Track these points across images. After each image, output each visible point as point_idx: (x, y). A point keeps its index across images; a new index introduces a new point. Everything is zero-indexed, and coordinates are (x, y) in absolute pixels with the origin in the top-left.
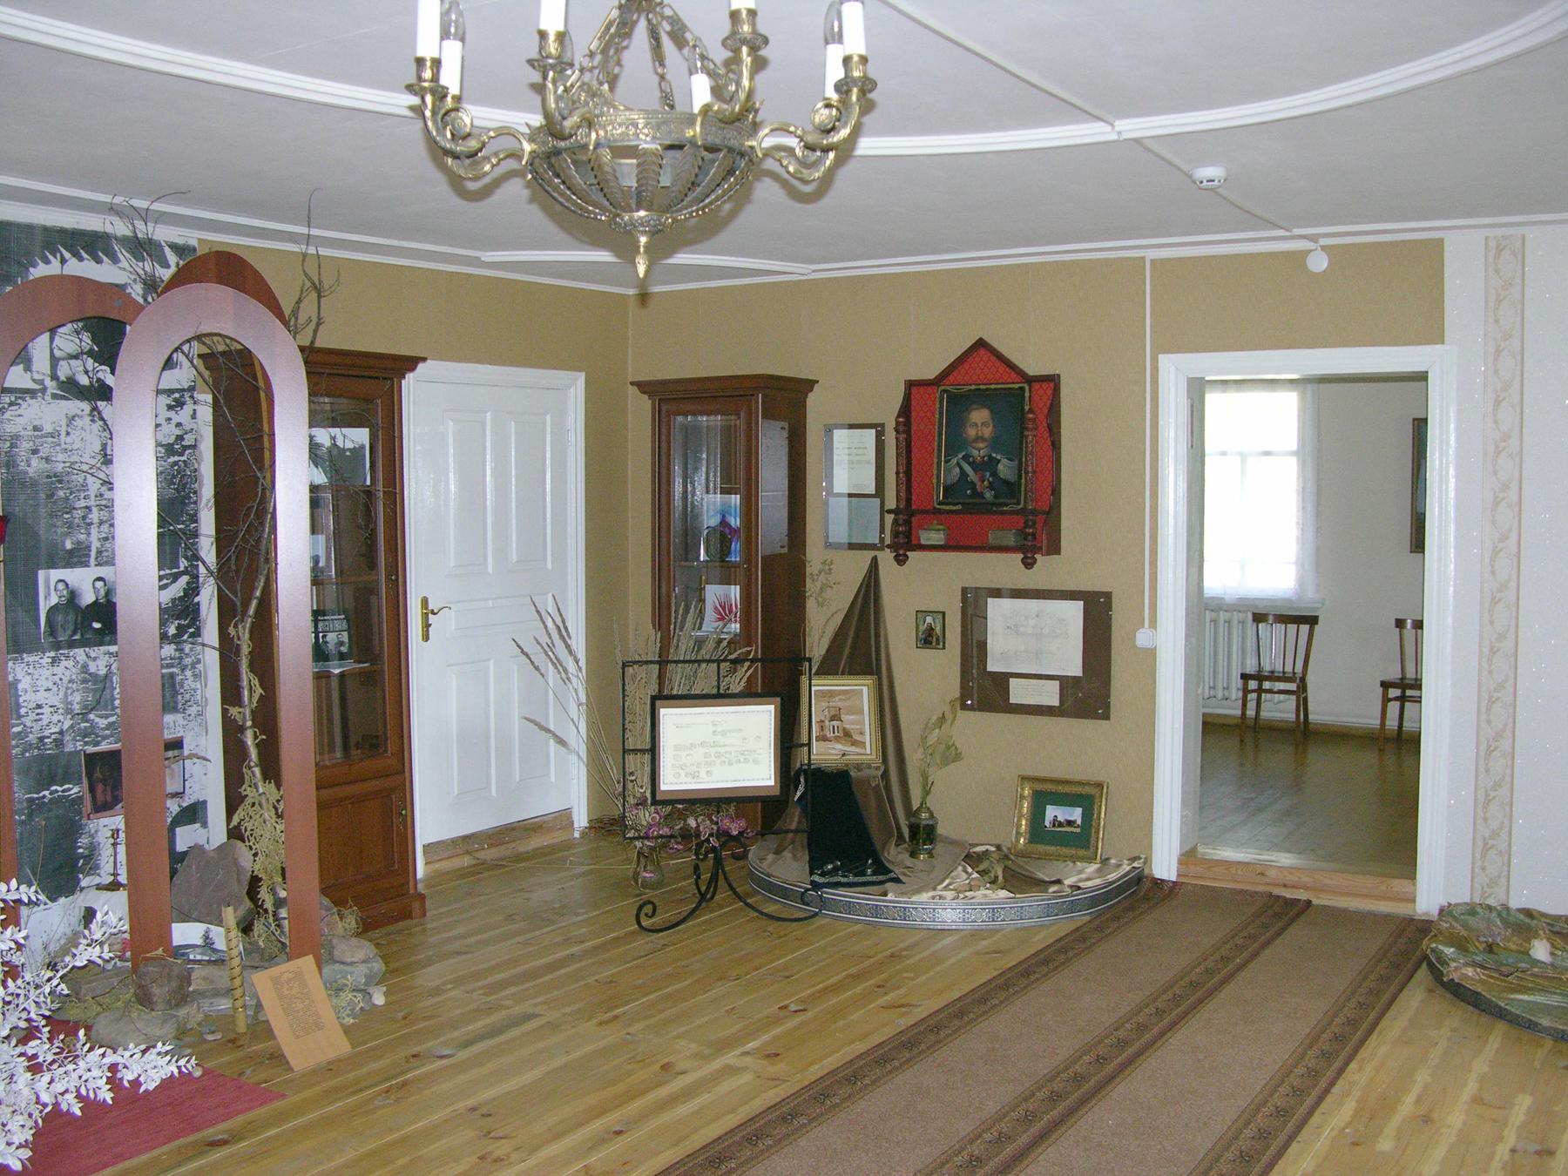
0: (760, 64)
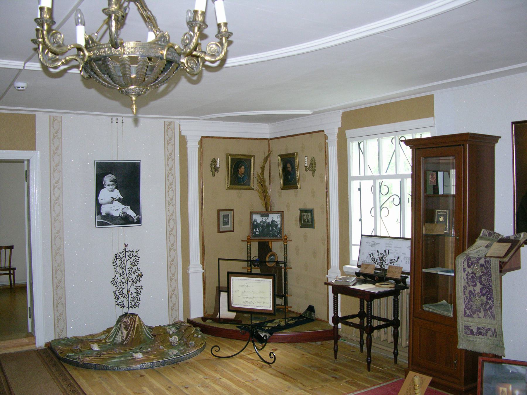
0: (230, 43)
